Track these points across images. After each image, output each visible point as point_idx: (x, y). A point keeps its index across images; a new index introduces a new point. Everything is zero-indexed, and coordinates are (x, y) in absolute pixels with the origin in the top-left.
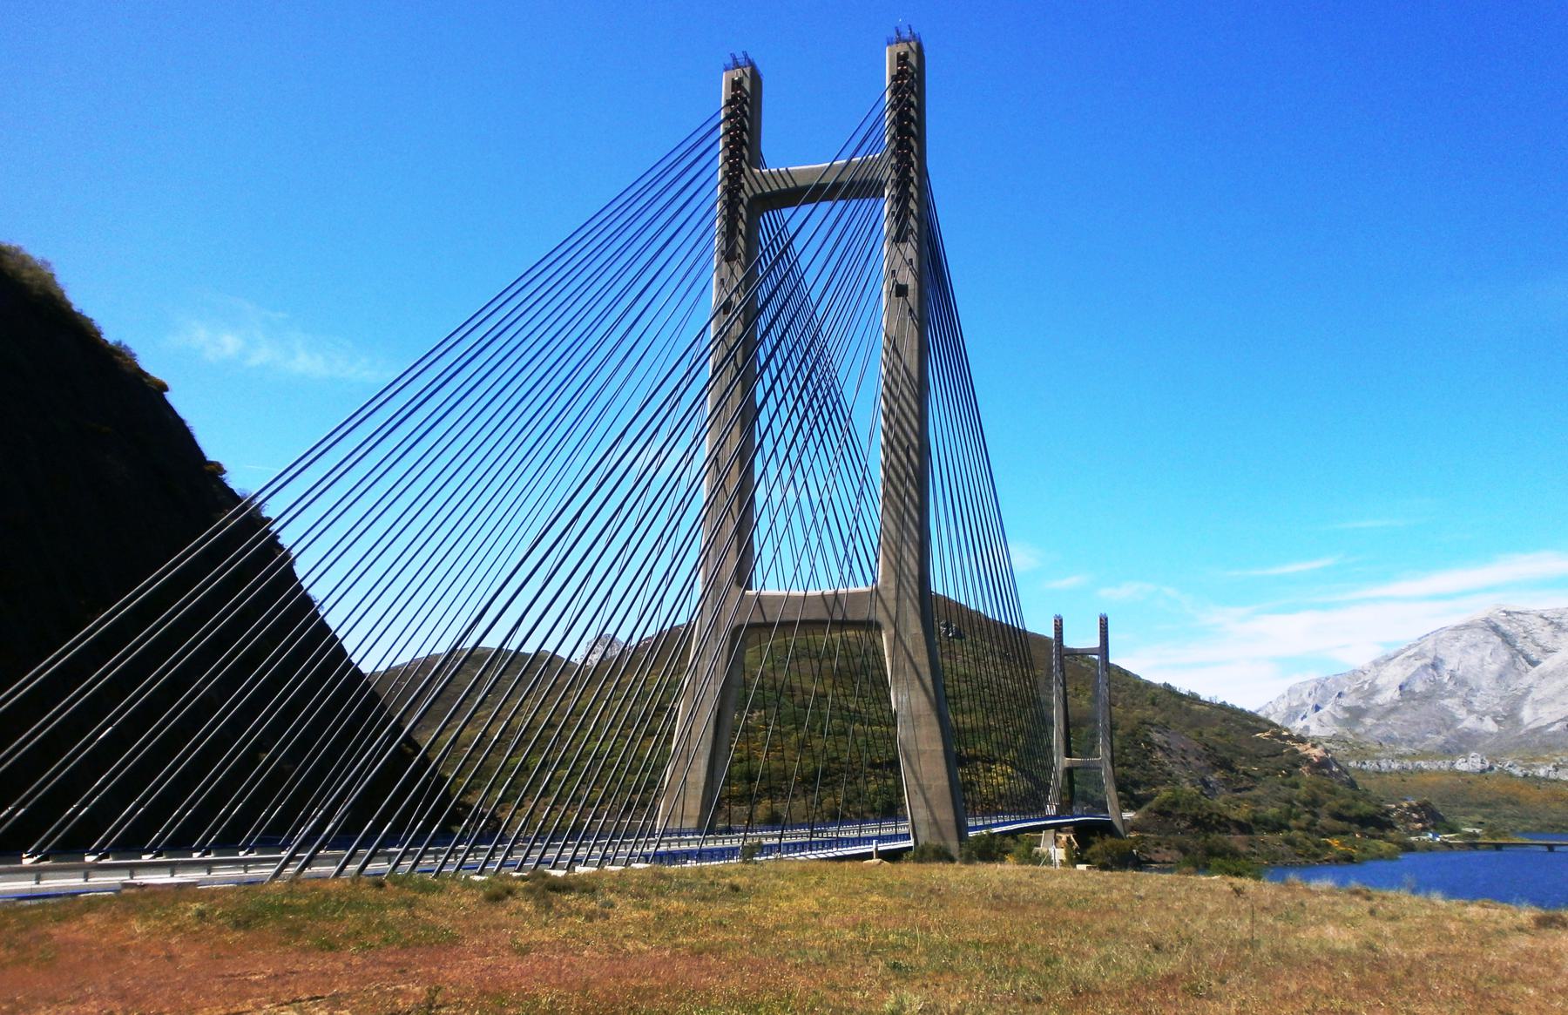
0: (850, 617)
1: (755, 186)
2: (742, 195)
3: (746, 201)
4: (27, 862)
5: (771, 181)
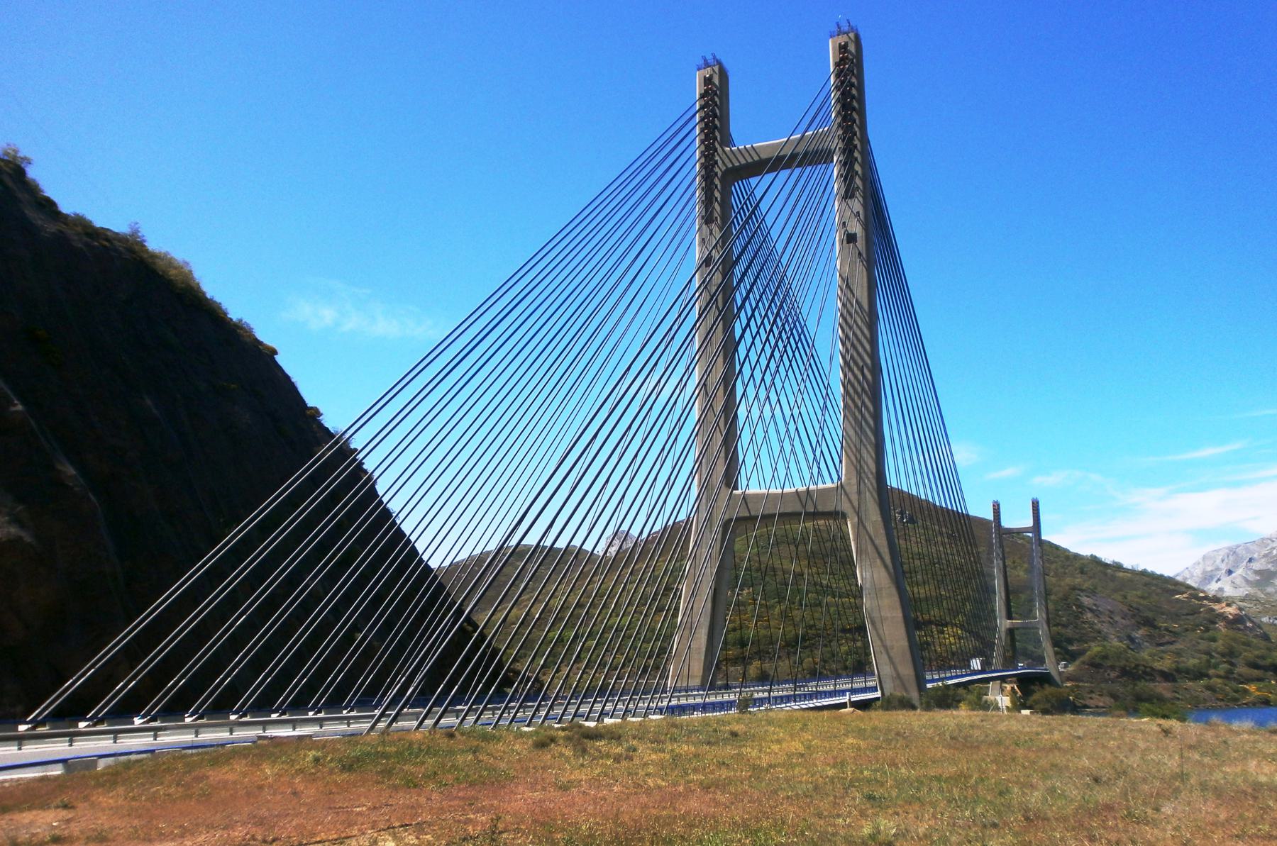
1: (726, 161)
2: (716, 169)
3: (720, 174)
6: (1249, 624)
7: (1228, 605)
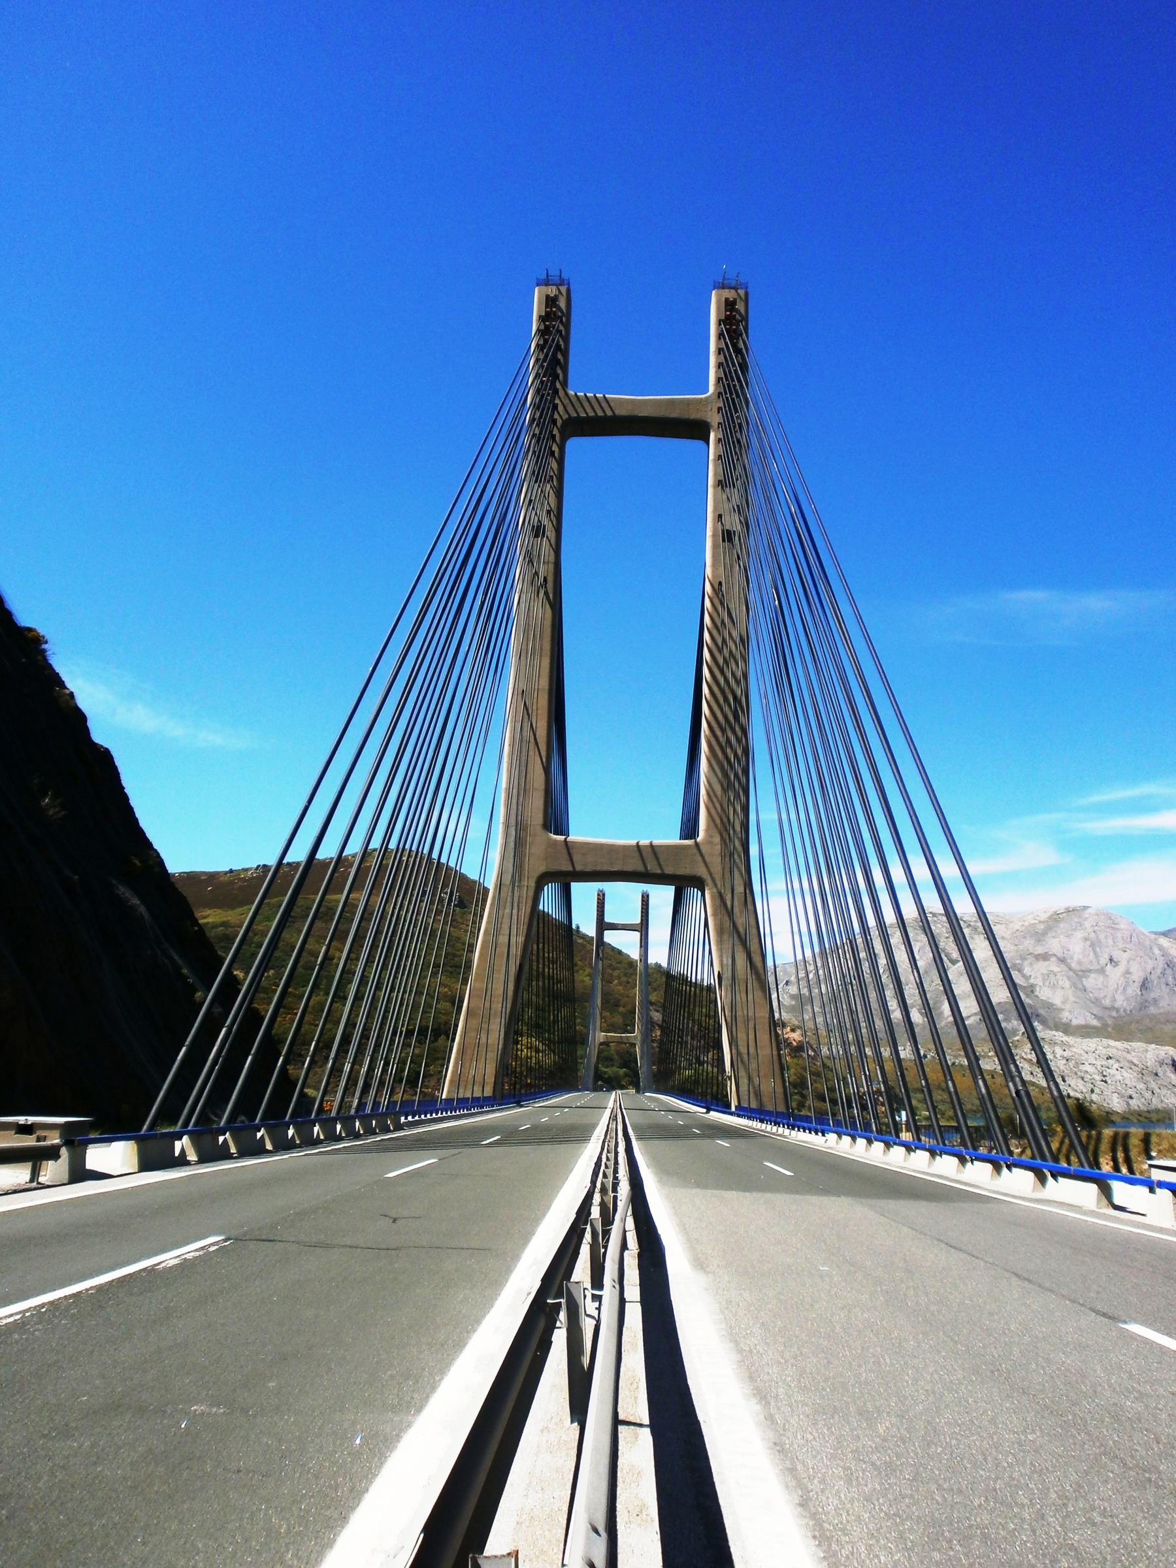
0: (579, 868)
1: (570, 409)
2: (556, 416)
3: (559, 423)
4: (982, 1151)
5: (586, 404)
7: (793, 1030)
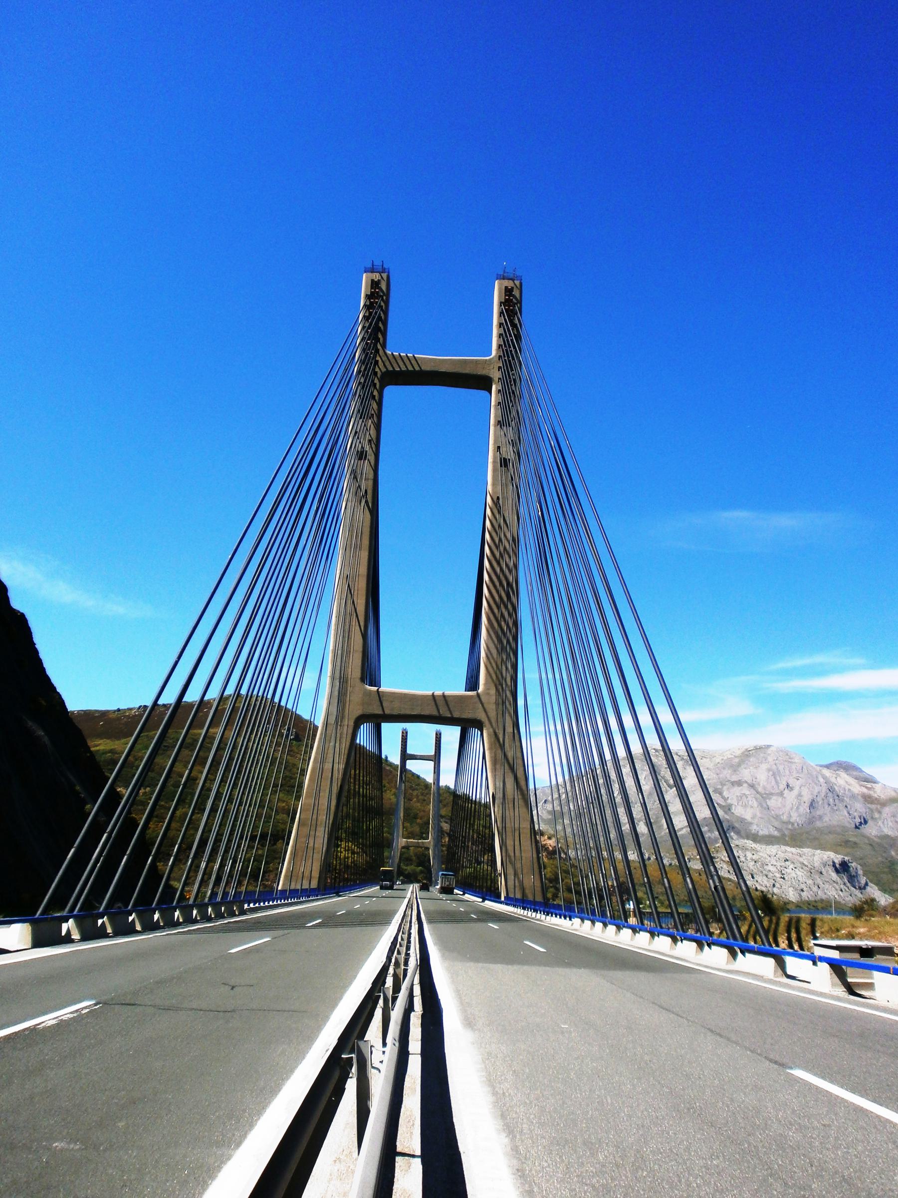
1: (387, 363)
2: (377, 370)
3: (379, 375)
6: (563, 855)
7: (549, 838)
